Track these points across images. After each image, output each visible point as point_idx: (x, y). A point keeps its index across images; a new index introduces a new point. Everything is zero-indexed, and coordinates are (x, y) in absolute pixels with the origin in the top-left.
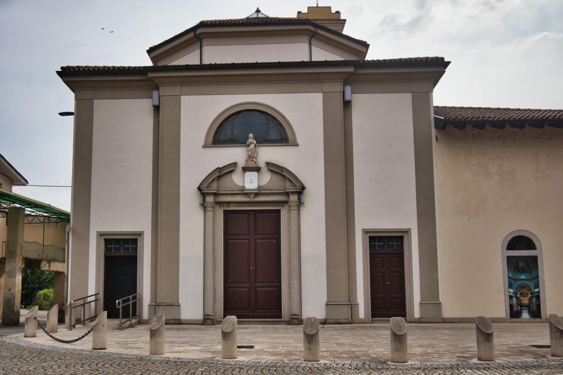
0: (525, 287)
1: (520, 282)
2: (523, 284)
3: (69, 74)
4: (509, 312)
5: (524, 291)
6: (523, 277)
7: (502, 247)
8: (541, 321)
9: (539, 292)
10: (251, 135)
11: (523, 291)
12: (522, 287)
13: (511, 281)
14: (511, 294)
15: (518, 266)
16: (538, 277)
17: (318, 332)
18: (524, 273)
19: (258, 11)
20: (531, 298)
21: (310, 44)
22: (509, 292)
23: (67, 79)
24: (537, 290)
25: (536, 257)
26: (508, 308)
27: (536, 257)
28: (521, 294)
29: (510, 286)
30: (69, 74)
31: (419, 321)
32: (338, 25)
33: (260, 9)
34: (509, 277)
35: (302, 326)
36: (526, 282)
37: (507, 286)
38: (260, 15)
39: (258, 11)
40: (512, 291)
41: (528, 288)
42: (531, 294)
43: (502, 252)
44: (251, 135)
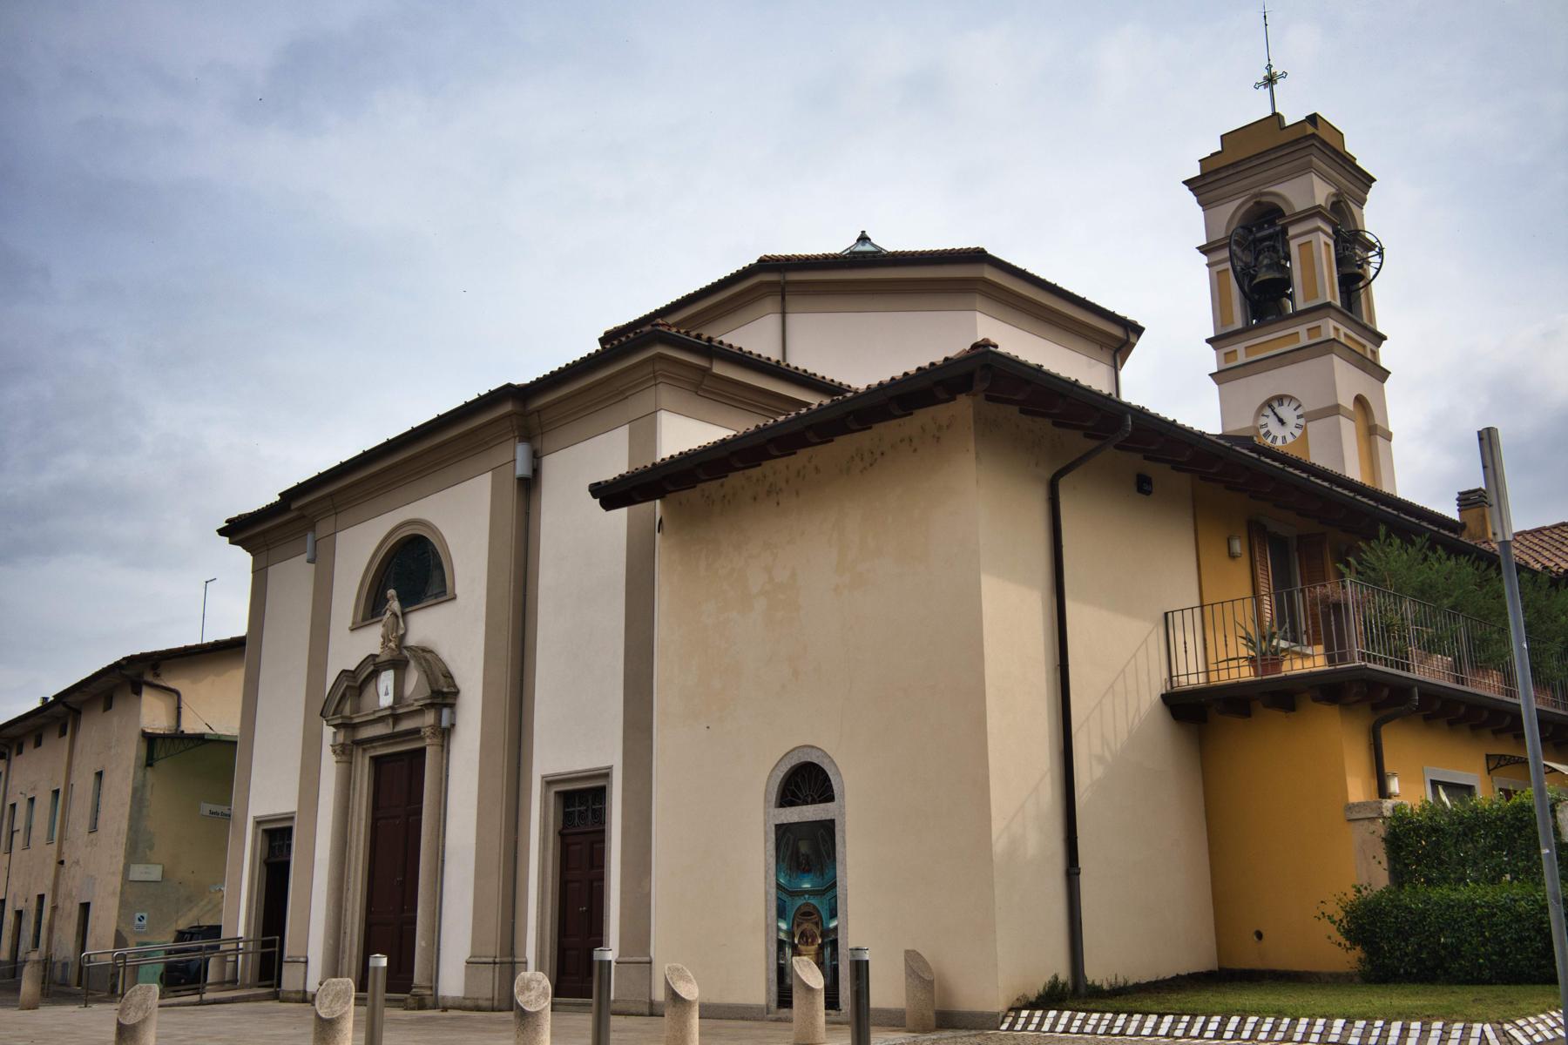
0: (810, 914)
1: (800, 902)
2: (807, 904)
3: (236, 530)
4: (774, 988)
5: (807, 926)
6: (807, 886)
7: (766, 800)
8: (839, 1019)
9: (836, 928)
10: (391, 592)
11: (805, 926)
12: (804, 914)
13: (784, 897)
14: (783, 936)
15: (798, 852)
16: (834, 885)
17: (144, 1021)
18: (809, 871)
19: (864, 238)
20: (821, 947)
21: (784, 313)
22: (779, 929)
23: (240, 537)
24: (833, 924)
25: (832, 821)
26: (774, 976)
27: (832, 821)
28: (803, 935)
29: (781, 914)
30: (236, 530)
31: (467, 1005)
32: (1297, 155)
33: (868, 234)
34: (779, 886)
35: (774, 1005)
36: (813, 901)
37: (774, 912)
38: (867, 248)
39: (864, 238)
40: (783, 926)
41: (815, 918)
42: (822, 936)
43: (766, 813)
44: (391, 592)
